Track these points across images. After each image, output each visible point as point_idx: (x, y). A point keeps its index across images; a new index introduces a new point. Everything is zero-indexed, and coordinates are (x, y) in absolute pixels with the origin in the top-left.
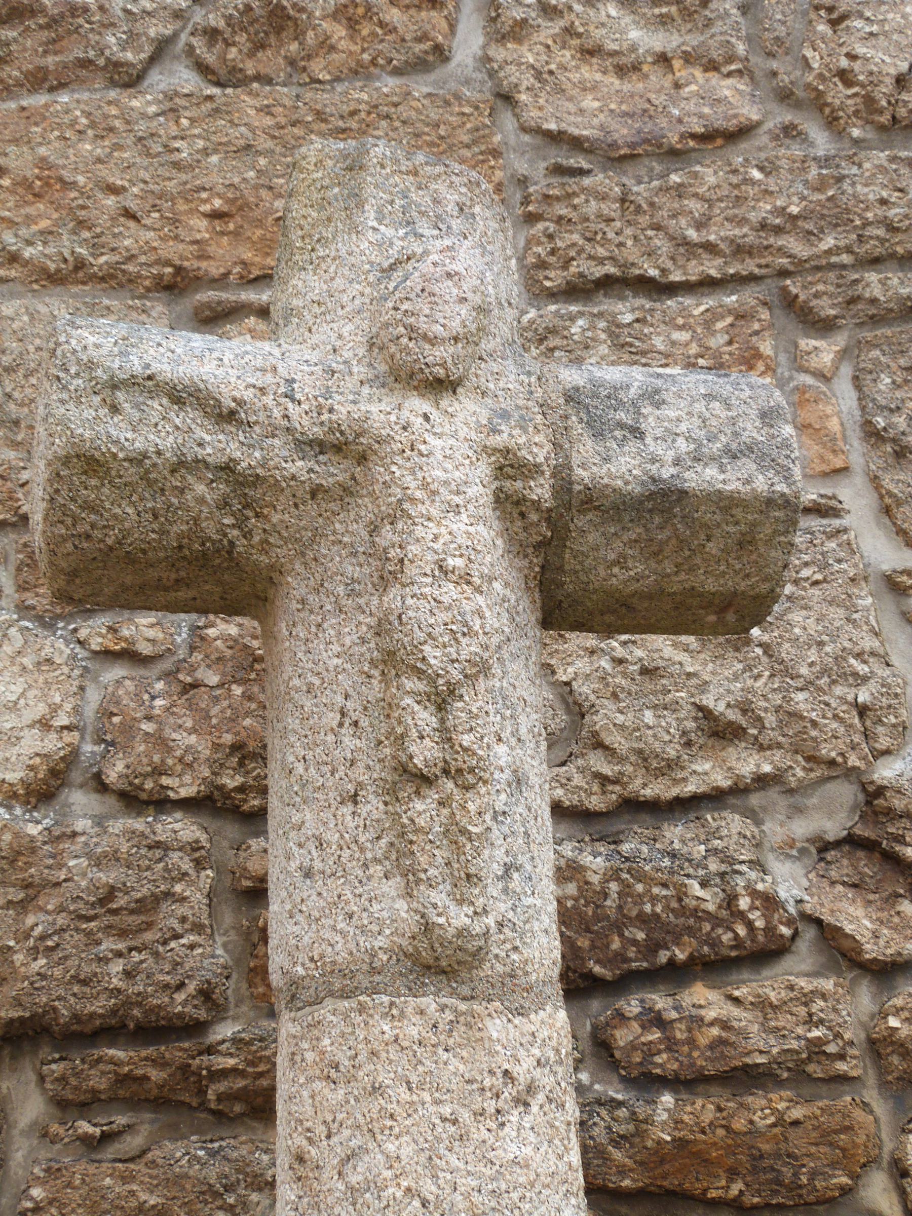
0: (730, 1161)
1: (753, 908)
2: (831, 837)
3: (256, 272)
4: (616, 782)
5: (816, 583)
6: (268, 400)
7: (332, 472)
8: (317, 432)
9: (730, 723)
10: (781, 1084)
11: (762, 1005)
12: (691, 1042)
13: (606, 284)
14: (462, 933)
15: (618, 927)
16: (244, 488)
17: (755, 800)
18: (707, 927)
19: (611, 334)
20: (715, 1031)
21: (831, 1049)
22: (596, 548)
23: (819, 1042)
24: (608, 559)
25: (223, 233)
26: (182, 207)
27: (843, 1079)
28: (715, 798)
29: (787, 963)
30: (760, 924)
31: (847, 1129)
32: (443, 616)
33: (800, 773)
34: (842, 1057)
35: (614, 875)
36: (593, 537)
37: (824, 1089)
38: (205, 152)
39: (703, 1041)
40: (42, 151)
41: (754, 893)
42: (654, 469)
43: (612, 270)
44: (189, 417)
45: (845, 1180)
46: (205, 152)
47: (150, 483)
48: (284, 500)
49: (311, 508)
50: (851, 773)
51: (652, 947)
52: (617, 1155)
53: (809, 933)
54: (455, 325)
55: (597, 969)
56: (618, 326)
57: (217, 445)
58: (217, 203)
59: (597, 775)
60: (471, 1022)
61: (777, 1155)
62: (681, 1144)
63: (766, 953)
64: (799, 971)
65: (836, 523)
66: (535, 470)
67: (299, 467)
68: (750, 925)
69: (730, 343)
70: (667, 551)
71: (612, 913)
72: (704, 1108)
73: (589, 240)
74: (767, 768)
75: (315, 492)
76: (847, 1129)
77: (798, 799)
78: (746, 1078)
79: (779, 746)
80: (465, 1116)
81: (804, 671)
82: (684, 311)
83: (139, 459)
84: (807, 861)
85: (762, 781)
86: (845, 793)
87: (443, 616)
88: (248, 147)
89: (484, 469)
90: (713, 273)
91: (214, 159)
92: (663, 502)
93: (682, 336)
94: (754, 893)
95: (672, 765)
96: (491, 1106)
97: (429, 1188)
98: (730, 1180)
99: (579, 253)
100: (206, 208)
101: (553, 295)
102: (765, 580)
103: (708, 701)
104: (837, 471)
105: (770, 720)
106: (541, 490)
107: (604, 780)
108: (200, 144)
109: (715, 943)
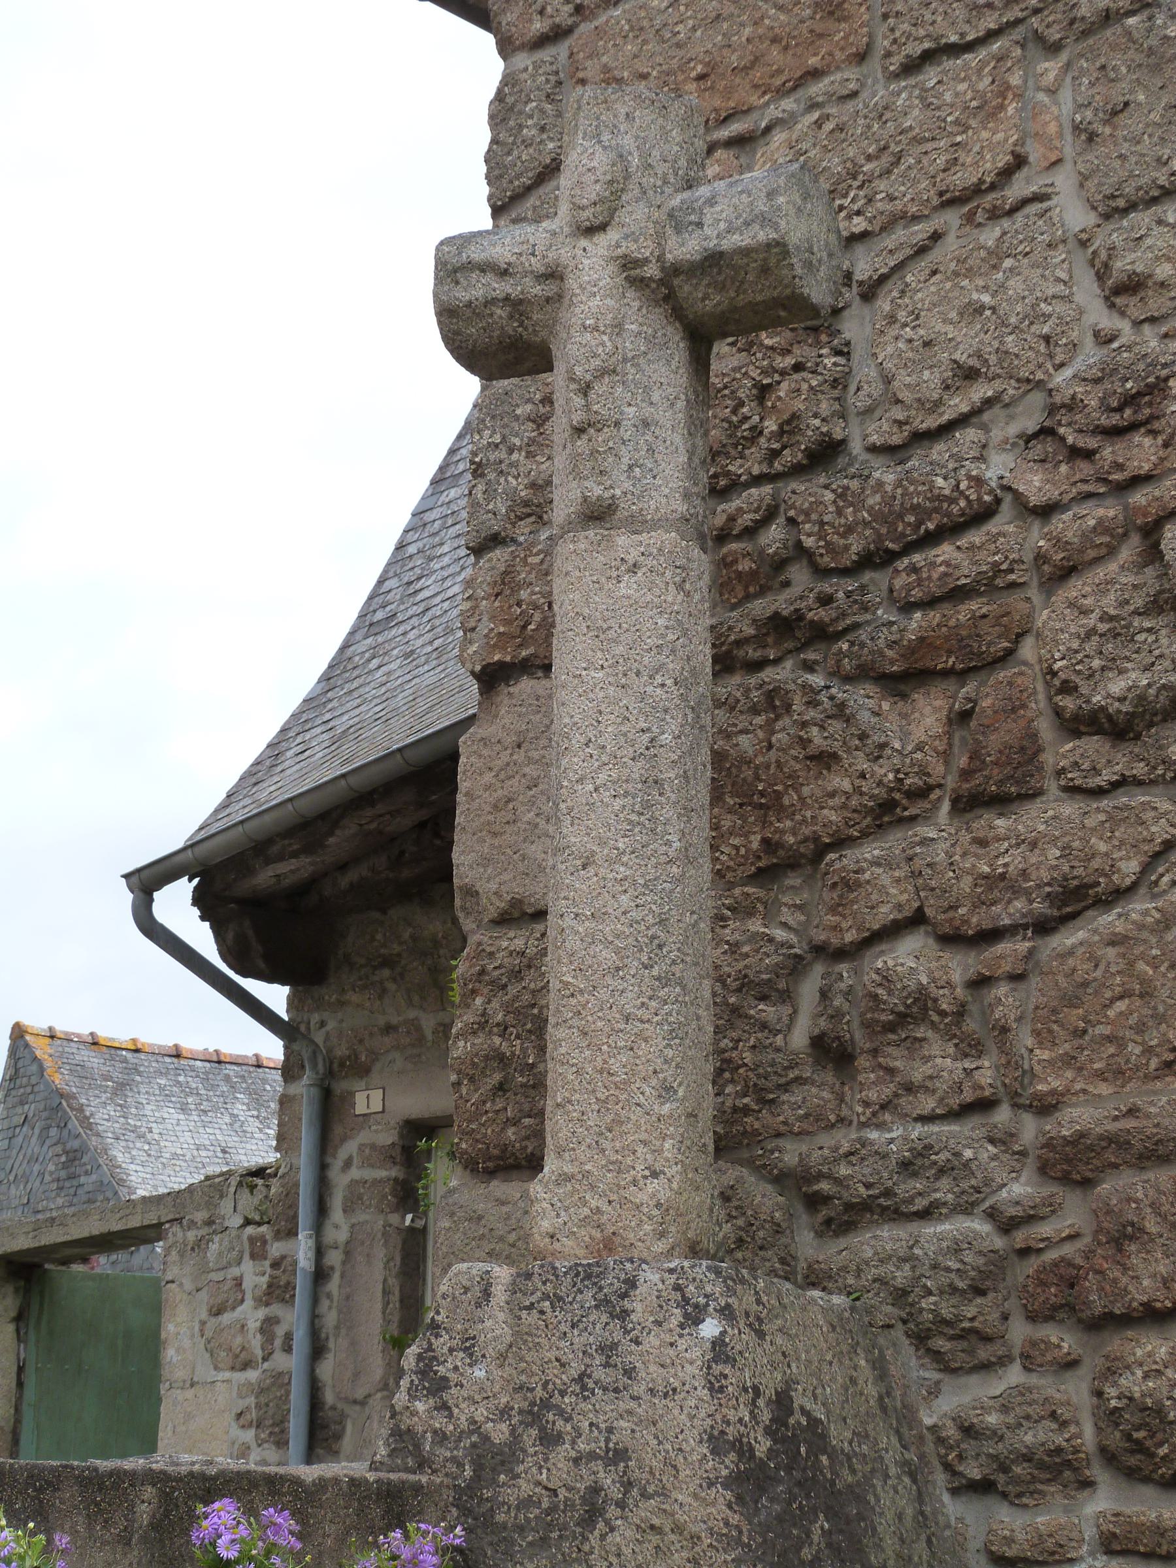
0: (946, 646)
1: (969, 488)
2: (1030, 432)
3: (724, 114)
4: (906, 423)
5: (1027, 254)
6: (523, 259)
7: (550, 289)
8: (542, 270)
9: (971, 368)
10: (981, 594)
11: (972, 548)
12: (929, 578)
13: (928, 57)
14: (599, 498)
15: (901, 516)
16: (517, 306)
17: (986, 416)
18: (945, 505)
19: (922, 99)
20: (942, 569)
21: (1004, 567)
22: (690, 293)
23: (996, 564)
24: (705, 300)
25: (705, 90)
26: (681, 77)
27: (1013, 585)
28: (962, 421)
29: (997, 519)
30: (973, 497)
31: (1008, 614)
32: (583, 350)
33: (1011, 392)
34: (1011, 571)
35: (899, 484)
36: (686, 288)
37: (1005, 593)
38: (694, 29)
39: (935, 576)
40: (604, 59)
41: (970, 478)
42: (705, 244)
43: (927, 45)
44: (489, 278)
45: (1007, 644)
46: (694, 29)
47: (478, 315)
48: (536, 308)
49: (549, 308)
50: (1040, 384)
51: (919, 523)
52: (890, 653)
53: (1008, 498)
54: (593, 197)
55: (891, 546)
56: (927, 90)
57: (501, 288)
58: (699, 68)
59: (895, 421)
60: (608, 539)
61: (970, 636)
62: (922, 639)
63: (983, 515)
64: (1003, 523)
65: (1045, 205)
66: (646, 261)
67: (537, 290)
68: (967, 498)
69: (993, 82)
70: (728, 283)
71: (897, 508)
72: (935, 616)
73: (915, 25)
74: (990, 393)
75: (548, 300)
76: (1008, 614)
77: (1011, 410)
78: (958, 594)
79: (999, 376)
80: (603, 580)
81: (1013, 320)
82: (966, 65)
83: (469, 304)
84: (1017, 451)
85: (988, 403)
86: (1037, 398)
87: (583, 350)
88: (719, 16)
89: (612, 268)
90: (992, 26)
91: (699, 33)
92: (714, 260)
93: (962, 87)
94: (970, 478)
95: (938, 403)
96: (614, 574)
97: (586, 611)
98: (948, 657)
99: (908, 38)
100: (693, 74)
101: (896, 76)
102: (786, 286)
103: (957, 356)
104: (1054, 164)
105: (993, 359)
106: (652, 271)
107: (900, 424)
108: (691, 22)
109: (948, 514)
